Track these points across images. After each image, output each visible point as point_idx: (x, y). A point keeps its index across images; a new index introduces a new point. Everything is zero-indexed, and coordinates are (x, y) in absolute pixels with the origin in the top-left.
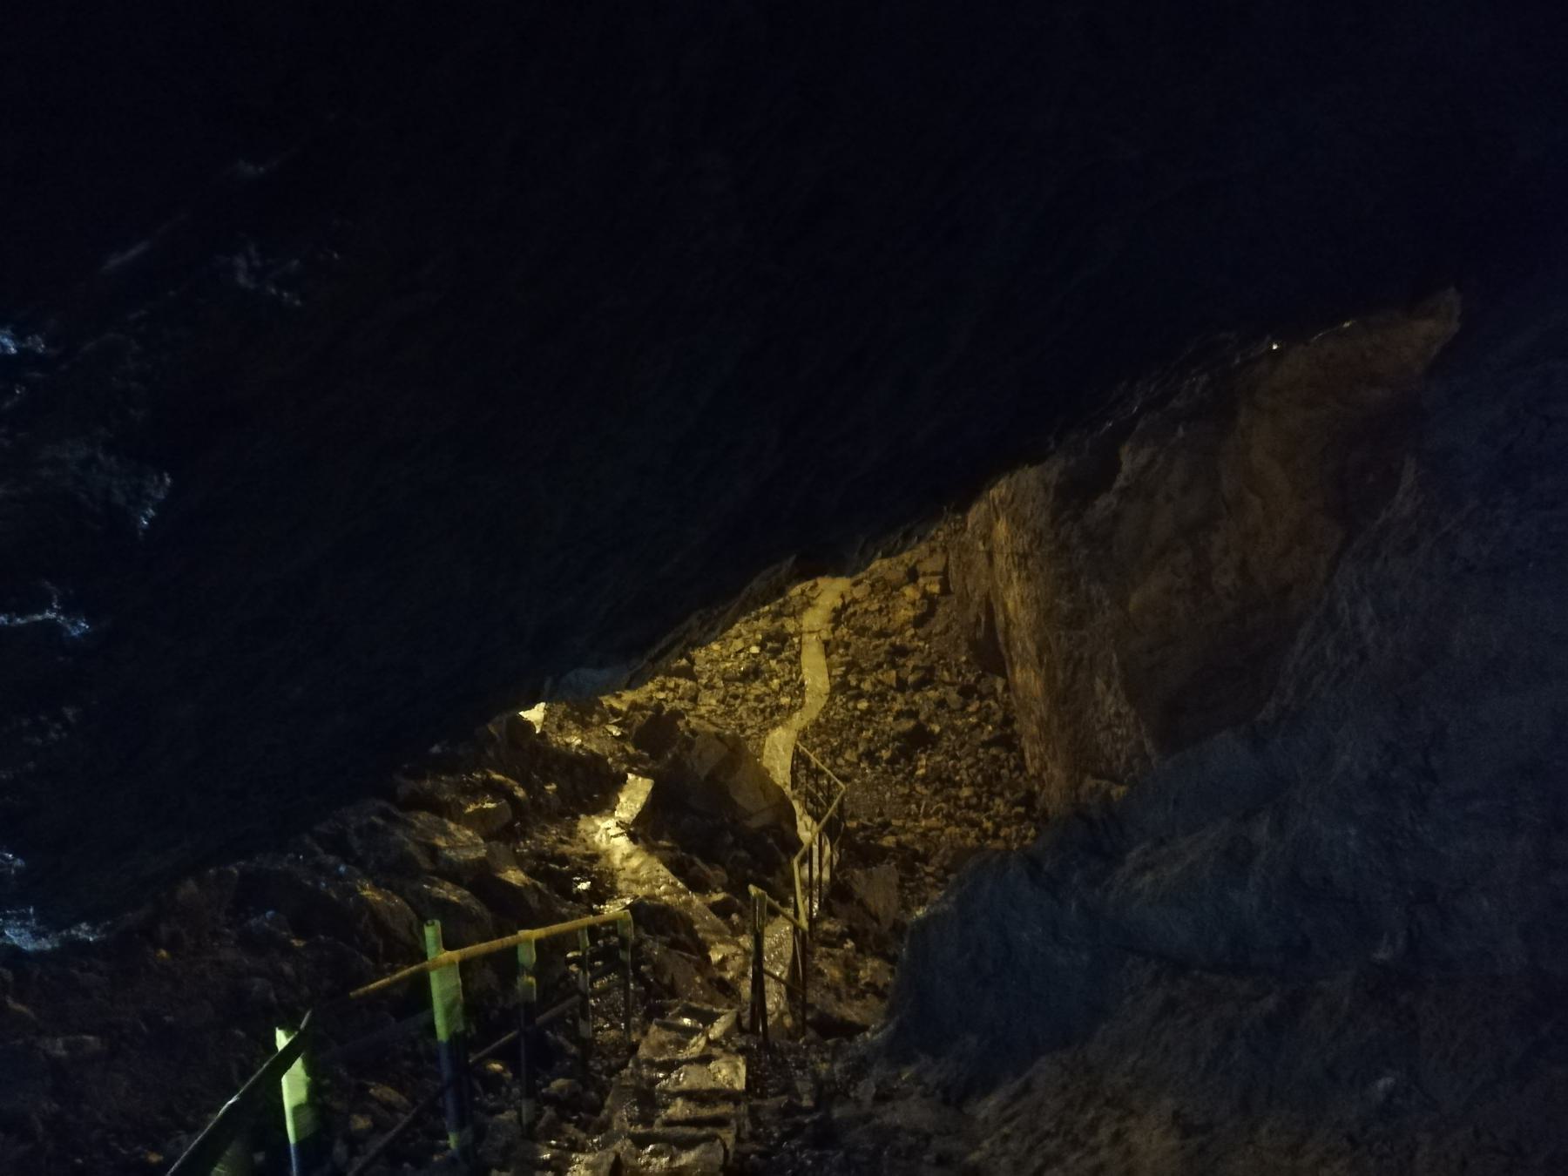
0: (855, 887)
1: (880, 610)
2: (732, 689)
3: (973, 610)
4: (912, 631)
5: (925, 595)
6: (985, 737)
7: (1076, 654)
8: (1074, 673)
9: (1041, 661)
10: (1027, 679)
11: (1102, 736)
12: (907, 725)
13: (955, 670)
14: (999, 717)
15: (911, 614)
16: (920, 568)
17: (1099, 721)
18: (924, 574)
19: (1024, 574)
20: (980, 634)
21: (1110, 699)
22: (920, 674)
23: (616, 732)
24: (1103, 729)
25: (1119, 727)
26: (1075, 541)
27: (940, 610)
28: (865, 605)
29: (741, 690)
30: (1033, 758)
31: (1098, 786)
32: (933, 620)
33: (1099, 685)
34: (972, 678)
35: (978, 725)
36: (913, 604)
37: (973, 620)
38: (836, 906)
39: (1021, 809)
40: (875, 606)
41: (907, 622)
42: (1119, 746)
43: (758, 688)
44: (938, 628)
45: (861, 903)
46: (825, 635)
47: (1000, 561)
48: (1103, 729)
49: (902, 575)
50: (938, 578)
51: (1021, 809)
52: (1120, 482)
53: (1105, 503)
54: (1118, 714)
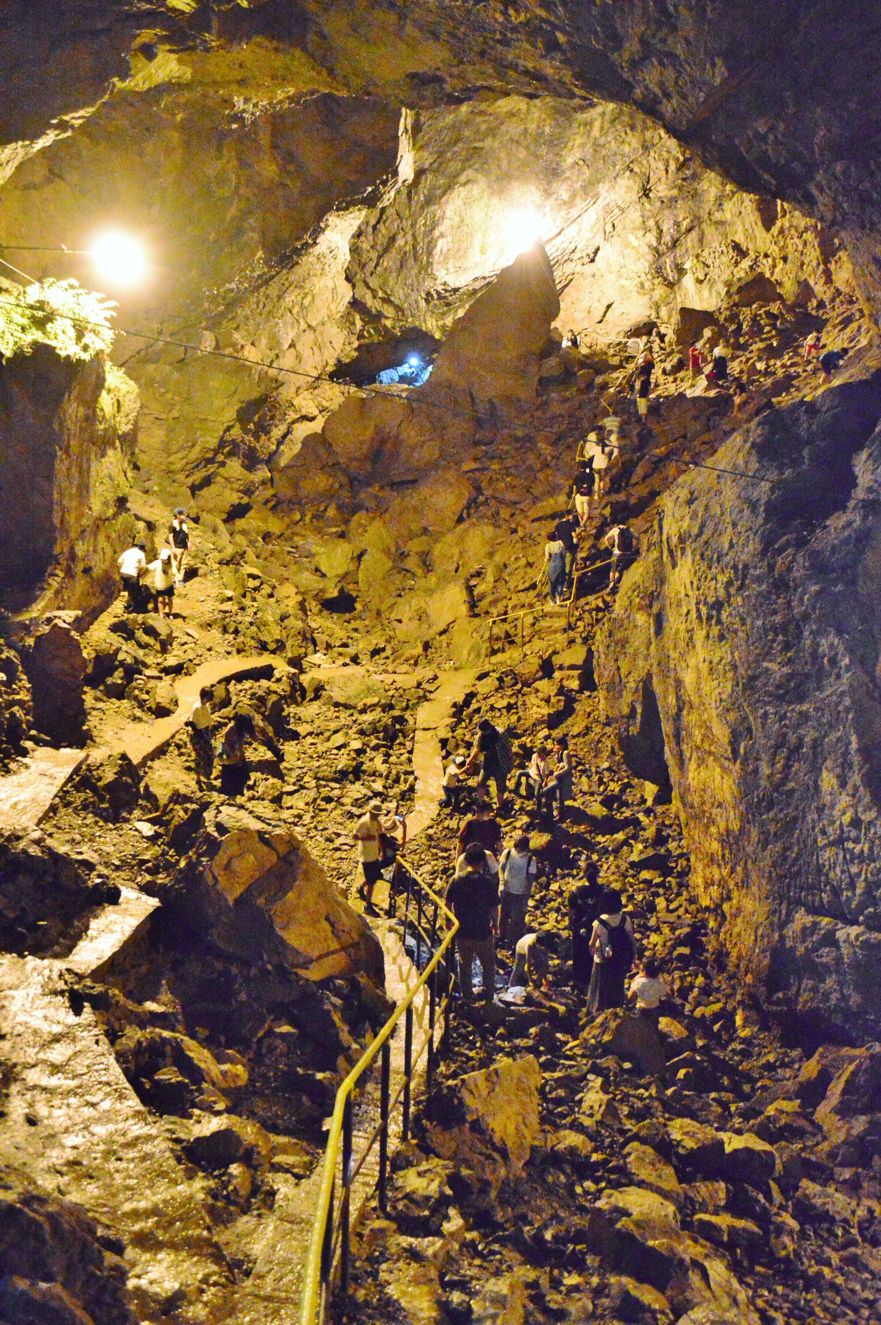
0: (469, 1100)
1: (509, 707)
2: (325, 792)
3: (627, 698)
4: (545, 732)
5: (561, 691)
6: (635, 857)
7: (792, 738)
8: (787, 767)
9: (735, 751)
10: (709, 780)
11: (828, 854)
13: (596, 778)
14: (650, 833)
15: (545, 711)
16: (556, 661)
17: (824, 832)
18: (561, 668)
19: (715, 631)
20: (634, 730)
21: (845, 800)
23: (147, 829)
24: (832, 844)
25: (856, 841)
26: (798, 573)
28: (492, 701)
29: (337, 792)
30: (708, 884)
31: (815, 924)
32: (570, 721)
33: (828, 780)
34: (614, 787)
35: (625, 843)
36: (547, 701)
37: (626, 711)
38: (437, 1136)
39: (686, 950)
40: (504, 703)
41: (539, 722)
42: (854, 869)
43: (356, 790)
44: (575, 730)
45: (478, 1127)
46: (444, 733)
47: (675, 623)
48: (832, 844)
50: (576, 673)
51: (686, 950)
52: (859, 494)
53: (839, 524)
54: (856, 823)
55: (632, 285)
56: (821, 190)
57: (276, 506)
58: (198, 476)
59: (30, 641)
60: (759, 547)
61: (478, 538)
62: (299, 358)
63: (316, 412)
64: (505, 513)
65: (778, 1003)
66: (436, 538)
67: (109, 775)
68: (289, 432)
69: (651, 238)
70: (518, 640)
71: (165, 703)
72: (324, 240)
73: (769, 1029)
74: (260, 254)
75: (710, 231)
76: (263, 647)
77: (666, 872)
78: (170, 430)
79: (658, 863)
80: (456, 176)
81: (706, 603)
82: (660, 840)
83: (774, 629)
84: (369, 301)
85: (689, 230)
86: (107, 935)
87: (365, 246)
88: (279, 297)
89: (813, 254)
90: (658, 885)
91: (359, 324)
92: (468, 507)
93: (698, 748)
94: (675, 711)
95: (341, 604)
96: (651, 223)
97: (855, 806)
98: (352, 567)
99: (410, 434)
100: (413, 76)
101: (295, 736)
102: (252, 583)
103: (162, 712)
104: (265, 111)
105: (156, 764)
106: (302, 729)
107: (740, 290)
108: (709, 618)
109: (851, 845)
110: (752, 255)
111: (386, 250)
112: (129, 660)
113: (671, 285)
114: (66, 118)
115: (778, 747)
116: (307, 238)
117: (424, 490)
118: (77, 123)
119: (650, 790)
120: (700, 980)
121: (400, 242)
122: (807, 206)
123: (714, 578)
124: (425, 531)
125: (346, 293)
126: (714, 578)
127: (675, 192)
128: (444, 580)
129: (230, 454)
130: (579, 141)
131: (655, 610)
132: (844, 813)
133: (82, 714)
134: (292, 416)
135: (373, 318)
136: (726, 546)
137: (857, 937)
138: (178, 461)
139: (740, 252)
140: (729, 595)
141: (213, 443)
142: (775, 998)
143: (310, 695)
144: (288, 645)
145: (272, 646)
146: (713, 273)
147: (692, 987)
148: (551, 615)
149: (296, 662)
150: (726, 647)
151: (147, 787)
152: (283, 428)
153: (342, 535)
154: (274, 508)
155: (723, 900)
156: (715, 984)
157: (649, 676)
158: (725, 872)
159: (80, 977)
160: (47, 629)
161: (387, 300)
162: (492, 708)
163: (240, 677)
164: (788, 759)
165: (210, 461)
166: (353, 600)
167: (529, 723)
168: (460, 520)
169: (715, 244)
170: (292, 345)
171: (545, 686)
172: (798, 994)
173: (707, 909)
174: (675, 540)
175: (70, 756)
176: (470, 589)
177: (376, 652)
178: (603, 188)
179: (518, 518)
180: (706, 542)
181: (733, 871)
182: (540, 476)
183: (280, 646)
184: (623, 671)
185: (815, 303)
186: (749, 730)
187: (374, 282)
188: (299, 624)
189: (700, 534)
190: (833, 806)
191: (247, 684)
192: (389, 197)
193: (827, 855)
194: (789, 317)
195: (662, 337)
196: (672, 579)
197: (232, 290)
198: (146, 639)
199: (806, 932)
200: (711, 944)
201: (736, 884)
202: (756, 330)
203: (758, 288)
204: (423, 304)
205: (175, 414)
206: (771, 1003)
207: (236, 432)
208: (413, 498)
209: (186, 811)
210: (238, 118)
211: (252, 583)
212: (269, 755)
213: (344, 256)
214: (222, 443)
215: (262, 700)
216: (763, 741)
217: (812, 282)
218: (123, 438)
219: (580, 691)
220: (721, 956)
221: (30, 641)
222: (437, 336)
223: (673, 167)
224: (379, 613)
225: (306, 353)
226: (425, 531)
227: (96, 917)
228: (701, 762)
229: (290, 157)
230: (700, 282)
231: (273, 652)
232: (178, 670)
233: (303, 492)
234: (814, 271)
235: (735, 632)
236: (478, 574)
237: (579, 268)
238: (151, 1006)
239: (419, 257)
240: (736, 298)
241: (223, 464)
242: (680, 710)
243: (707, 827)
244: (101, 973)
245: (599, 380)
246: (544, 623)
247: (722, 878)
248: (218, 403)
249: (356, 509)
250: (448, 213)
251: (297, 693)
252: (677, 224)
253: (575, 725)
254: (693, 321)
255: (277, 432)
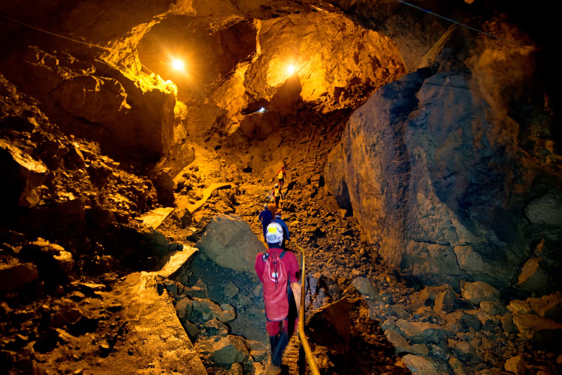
1: (299, 193)
4: (311, 199)
5: (314, 187)
9: (383, 192)
12: (314, 229)
14: (346, 225)
16: (312, 179)
19: (373, 154)
20: (340, 194)
21: (428, 202)
22: (315, 212)
27: (319, 191)
29: (252, 219)
30: (372, 236)
36: (310, 190)
37: (337, 188)
39: (365, 258)
41: (309, 196)
42: (433, 225)
44: (319, 198)
47: (356, 156)
49: (306, 181)
51: (365, 258)
54: (433, 209)
55: (320, 83)
56: (389, 25)
57: (228, 146)
58: (206, 138)
59: (156, 177)
60: (389, 123)
61: (284, 150)
62: (232, 107)
63: (237, 121)
64: (291, 143)
65: (405, 273)
66: (273, 151)
67: (181, 215)
68: (231, 126)
69: (325, 70)
70: (300, 175)
71: (199, 196)
72: (236, 75)
73: (401, 282)
74: (220, 75)
75: (341, 66)
76: (228, 180)
77: (353, 236)
78: (197, 125)
79: (350, 233)
80: (271, 56)
81: (369, 146)
82: (349, 227)
83: (396, 149)
84: (250, 92)
85: (335, 67)
86: (176, 262)
87: (248, 76)
88: (226, 90)
89: (370, 69)
90: (351, 240)
91: (248, 98)
92: (281, 143)
93: (366, 194)
94: (357, 184)
95: (248, 170)
96: (325, 66)
97: (432, 203)
98: (250, 160)
99: (264, 125)
100: (262, 6)
101: (238, 204)
102: (223, 164)
103: (198, 199)
104: (219, 29)
105: (197, 213)
106: (240, 202)
107: (351, 81)
108: (371, 150)
109: (431, 217)
110: (353, 72)
111: (254, 77)
112: (188, 184)
113: (331, 83)
114: (158, 16)
115: (400, 187)
116: (233, 70)
117: (269, 139)
118: (162, 18)
119: (343, 212)
120: (371, 268)
121: (258, 75)
122: (384, 31)
123: (372, 137)
124: (270, 150)
125: (244, 89)
126: (372, 137)
127: (331, 57)
128: (277, 162)
129: (214, 132)
130: (304, 44)
131: (348, 154)
132: (428, 206)
133: (173, 199)
134: (231, 123)
135: (251, 96)
136: (376, 126)
137: (436, 248)
138: (200, 133)
139: (350, 71)
140: (378, 141)
141: (210, 128)
142: (404, 271)
143: (242, 193)
144: (235, 179)
145: (230, 180)
146: (342, 78)
147: (369, 270)
148: (309, 167)
149: (237, 184)
150: (377, 158)
151: (194, 219)
152: (229, 125)
153: (247, 152)
154: (228, 147)
155: (378, 240)
156: (376, 269)
157: (344, 177)
158: (379, 232)
159: (164, 278)
160: (161, 173)
161: (255, 91)
162: (294, 194)
163: (222, 188)
164: (404, 191)
165: (209, 133)
166: (252, 169)
167: (305, 197)
168: (279, 146)
169: (343, 70)
170: (230, 103)
171: (309, 186)
172: (413, 269)
173: (373, 244)
174: (355, 129)
175: (168, 210)
176: (285, 162)
177: (259, 181)
178: (311, 57)
179: (296, 144)
180: (368, 126)
181: (382, 230)
182: (301, 133)
183: (232, 180)
184: (336, 177)
185: (371, 83)
186: (388, 184)
187: (251, 87)
188: (237, 174)
189: (365, 125)
190: (423, 204)
191: (224, 190)
192: (255, 59)
193: (422, 221)
194: (365, 87)
195: (329, 96)
196: (354, 143)
197: (212, 86)
198: (193, 179)
199: (415, 248)
200: (374, 256)
201: (384, 235)
202: (356, 91)
203: (355, 80)
204: (265, 92)
205: (199, 120)
206: (403, 273)
207: (216, 125)
208: (266, 142)
209: (207, 222)
210: (210, 31)
211: (223, 164)
212: (231, 209)
213: (243, 79)
214: (212, 128)
215: (228, 194)
216: (394, 186)
217: (370, 77)
218: (183, 121)
219: (319, 187)
220: (379, 258)
221: (156, 177)
222: (269, 100)
223: (330, 50)
224: (259, 172)
225: (234, 105)
226: (270, 150)
227: (173, 255)
228: (367, 198)
229: (227, 47)
230: (339, 81)
231: (230, 181)
232: (203, 187)
233: (236, 143)
234: (371, 74)
235: (381, 153)
236: (286, 158)
237: (306, 81)
238: (195, 288)
239: (263, 79)
240: (350, 83)
241: (213, 134)
242: (358, 183)
243: (371, 218)
244: (173, 277)
245: (314, 108)
246: (307, 169)
247: (378, 234)
248: (211, 117)
249: (250, 145)
250: (270, 66)
251: (238, 193)
252: (332, 66)
253: (319, 196)
254: (338, 91)
255: (228, 126)
